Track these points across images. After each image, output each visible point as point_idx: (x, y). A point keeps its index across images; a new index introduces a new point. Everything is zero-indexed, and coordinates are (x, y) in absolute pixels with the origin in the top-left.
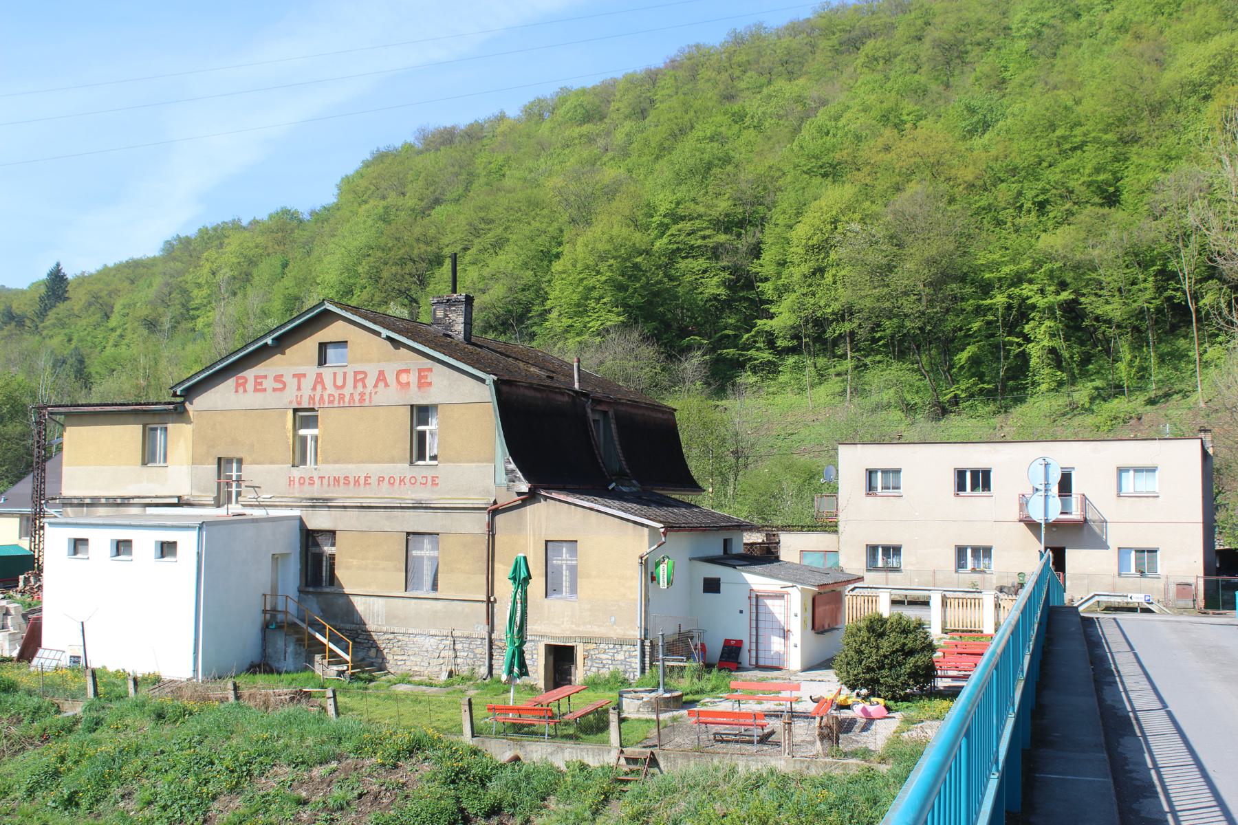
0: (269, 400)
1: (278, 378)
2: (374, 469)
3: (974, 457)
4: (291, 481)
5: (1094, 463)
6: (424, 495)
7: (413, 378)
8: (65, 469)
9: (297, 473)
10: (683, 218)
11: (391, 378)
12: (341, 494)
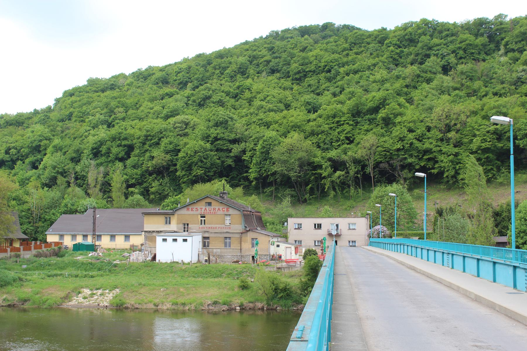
0: (194, 212)
1: (196, 209)
2: (218, 226)
3: (318, 221)
4: (200, 228)
5: (343, 223)
6: (228, 231)
7: (225, 209)
8: (145, 225)
9: (201, 226)
10: (219, 139)
11: (221, 209)
12: (210, 230)
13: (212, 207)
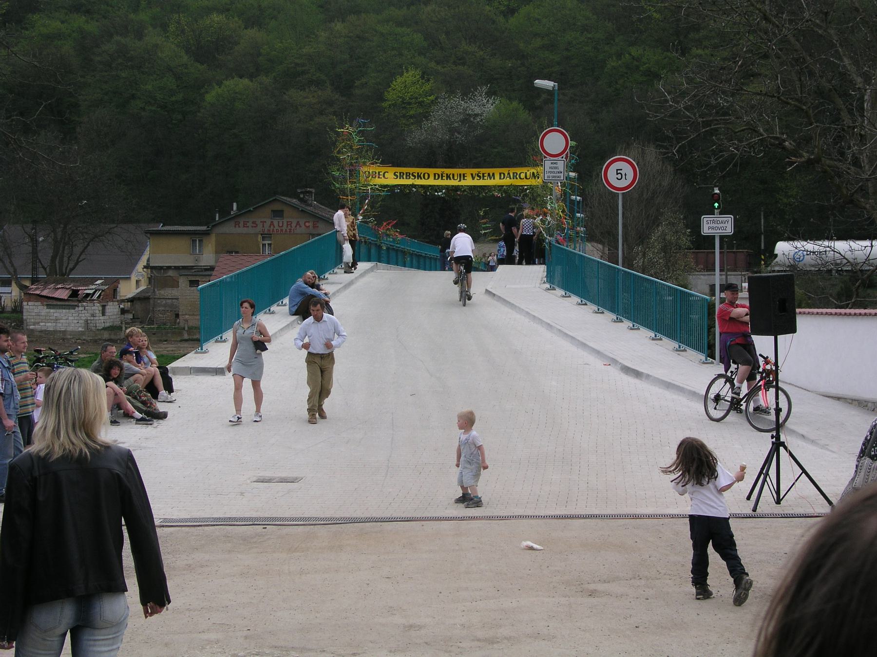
1: (253, 223)
7: (310, 224)
13: (285, 221)
